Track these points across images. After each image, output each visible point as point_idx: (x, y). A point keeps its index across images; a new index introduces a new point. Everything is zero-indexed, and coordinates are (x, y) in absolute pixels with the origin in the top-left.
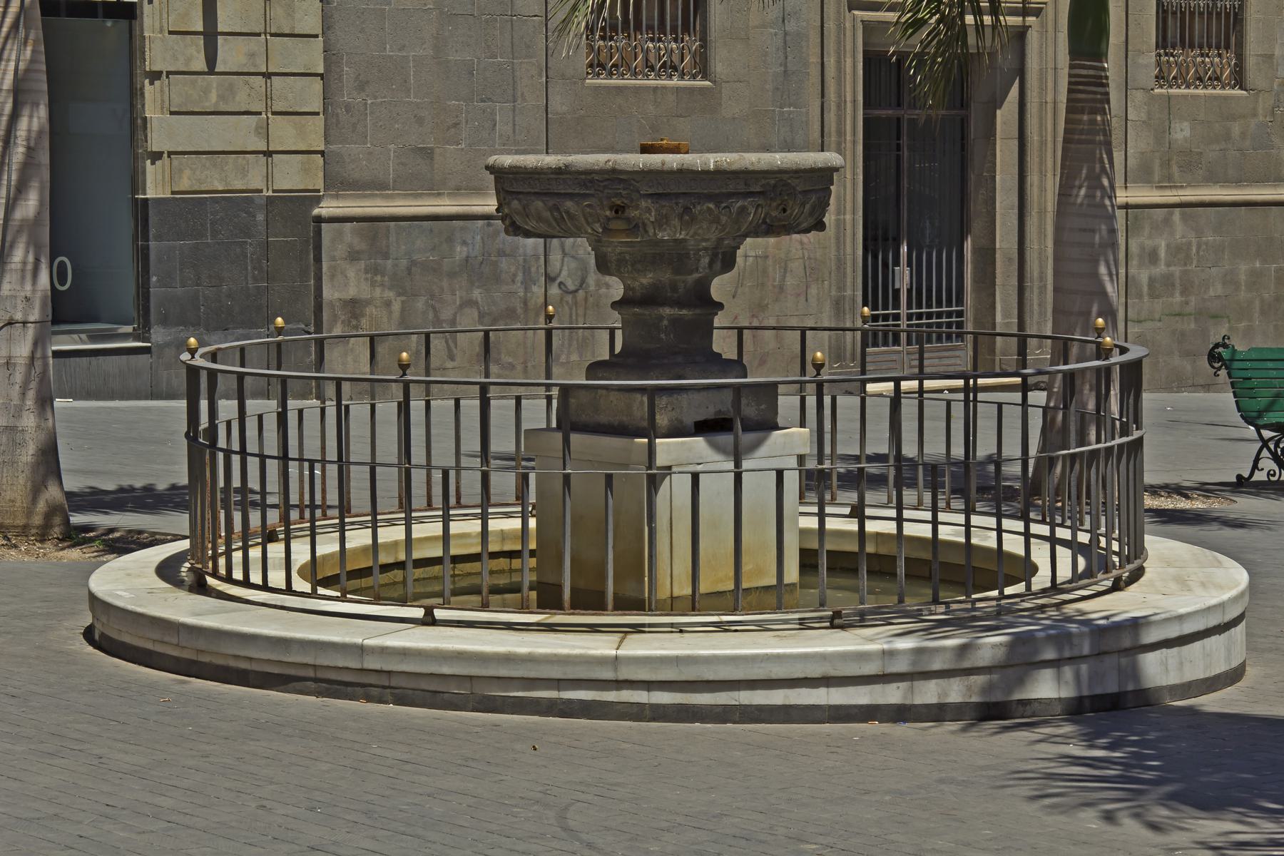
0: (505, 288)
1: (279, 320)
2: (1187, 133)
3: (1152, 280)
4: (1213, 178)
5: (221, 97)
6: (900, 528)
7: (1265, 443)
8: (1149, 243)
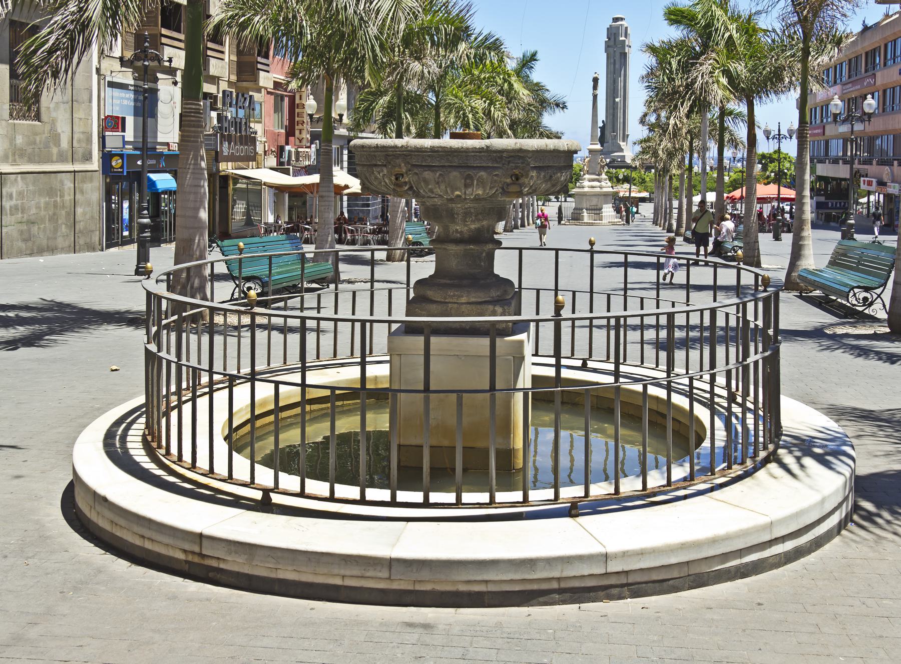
2: (21, 141)
3: (11, 207)
4: (31, 161)
6: (558, 372)
8: (9, 190)
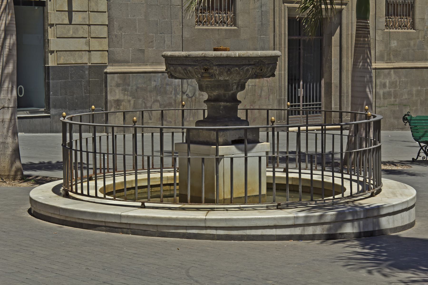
0: (168, 96)
1: (93, 106)
2: (396, 44)
3: (384, 93)
4: (404, 59)
5: (74, 32)
6: (300, 176)
7: (422, 148)
8: (383, 81)
